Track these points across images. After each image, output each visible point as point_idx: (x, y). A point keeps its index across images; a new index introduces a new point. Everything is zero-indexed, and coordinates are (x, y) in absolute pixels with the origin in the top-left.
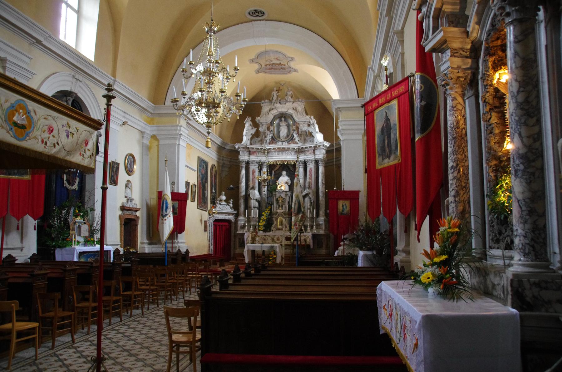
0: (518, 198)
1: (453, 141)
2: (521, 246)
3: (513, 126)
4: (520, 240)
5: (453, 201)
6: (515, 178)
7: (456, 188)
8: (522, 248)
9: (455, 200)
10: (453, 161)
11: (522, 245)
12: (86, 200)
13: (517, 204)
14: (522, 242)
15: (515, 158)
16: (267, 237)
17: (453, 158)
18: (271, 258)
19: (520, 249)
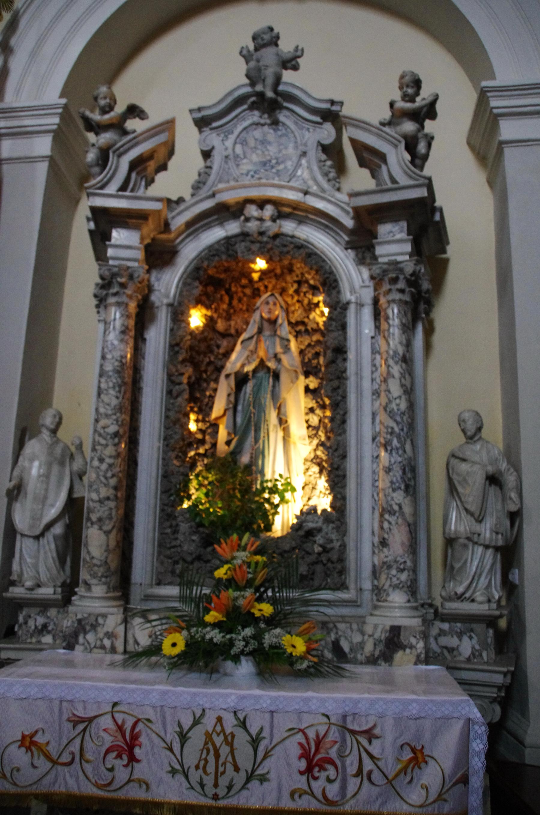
0: (408, 519)
1: (123, 389)
2: (409, 583)
3: (405, 429)
4: (409, 576)
5: (112, 497)
6: (405, 495)
7: (120, 475)
8: (410, 586)
9: (116, 496)
10: (120, 423)
11: (411, 582)
12: (91, 790)
13: (407, 529)
14: (411, 577)
15: (407, 469)
16: (292, 135)
17: (120, 420)
18: (211, 510)
19: (408, 587)
